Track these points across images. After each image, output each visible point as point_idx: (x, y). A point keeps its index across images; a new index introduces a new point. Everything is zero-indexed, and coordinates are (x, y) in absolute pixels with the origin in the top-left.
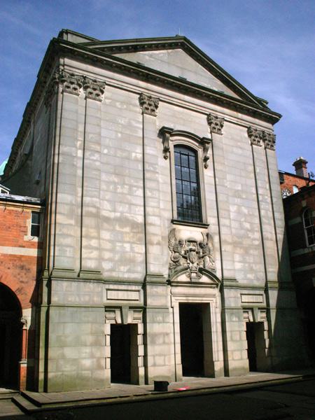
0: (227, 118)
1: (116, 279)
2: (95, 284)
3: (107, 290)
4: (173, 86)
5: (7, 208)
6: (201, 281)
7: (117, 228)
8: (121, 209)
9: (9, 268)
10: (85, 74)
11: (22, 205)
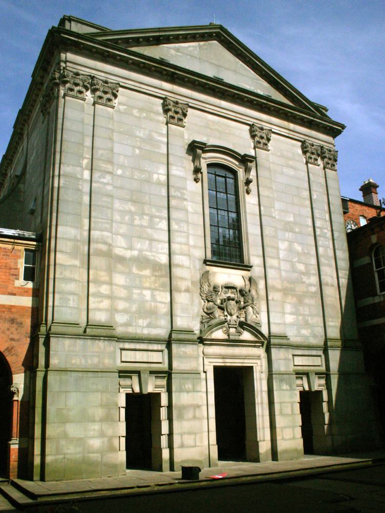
0: (192, 103)
7: (135, 270)
8: (139, 246)
11: (12, 240)
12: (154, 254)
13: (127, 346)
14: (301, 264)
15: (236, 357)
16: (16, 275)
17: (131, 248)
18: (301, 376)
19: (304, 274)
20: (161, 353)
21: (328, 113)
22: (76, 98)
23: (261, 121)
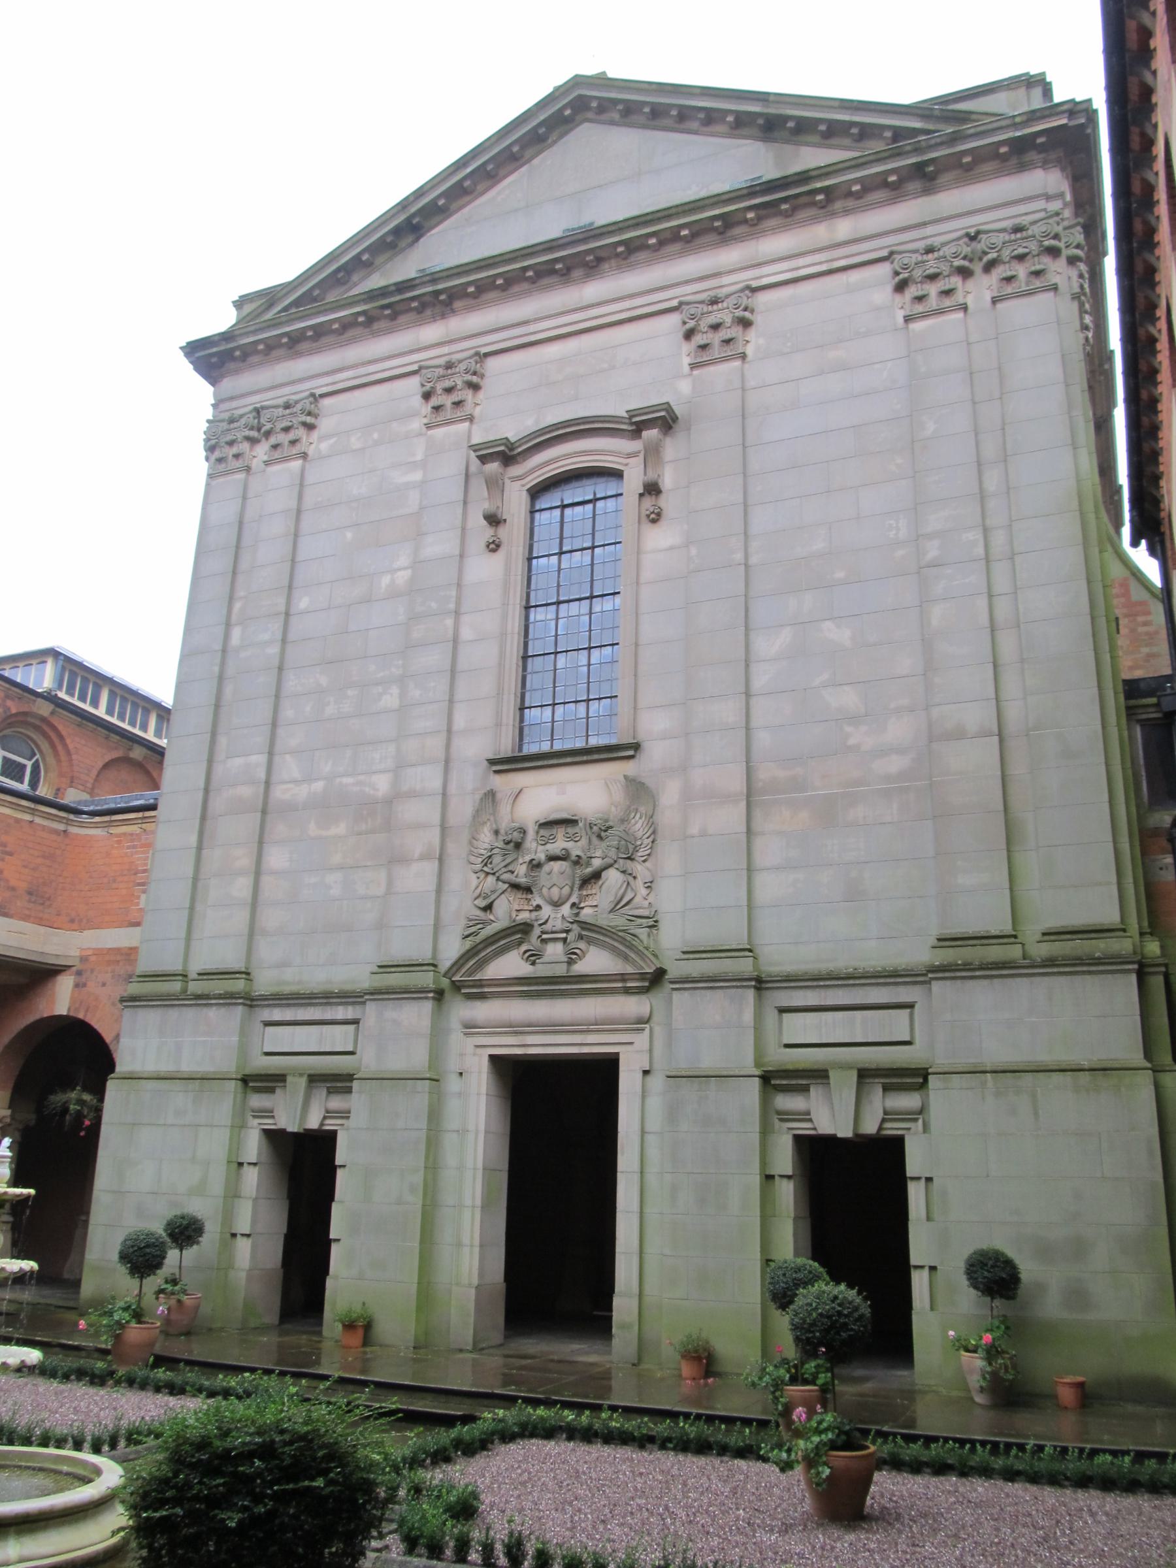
0: (321, 385)
1: (294, 988)
2: (223, 1010)
3: (783, 1010)
4: (968, 168)
5: (113, 830)
6: (580, 968)
7: (313, 830)
8: (327, 768)
9: (104, 985)
10: (256, 400)
11: (140, 815)
12: (362, 778)
13: (277, 1014)
14: (846, 688)
15: (557, 1029)
16: (143, 884)
17: (308, 779)
18: (804, 1082)
19: (854, 719)
20: (352, 1027)
21: (596, 225)
22: (940, 312)
23: (924, 224)
